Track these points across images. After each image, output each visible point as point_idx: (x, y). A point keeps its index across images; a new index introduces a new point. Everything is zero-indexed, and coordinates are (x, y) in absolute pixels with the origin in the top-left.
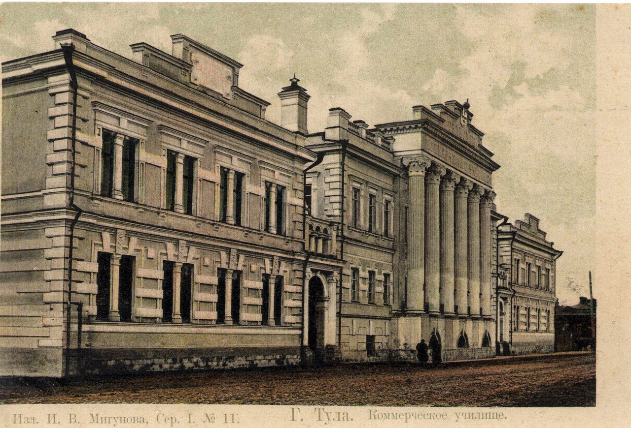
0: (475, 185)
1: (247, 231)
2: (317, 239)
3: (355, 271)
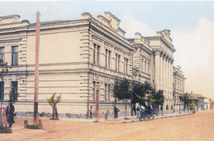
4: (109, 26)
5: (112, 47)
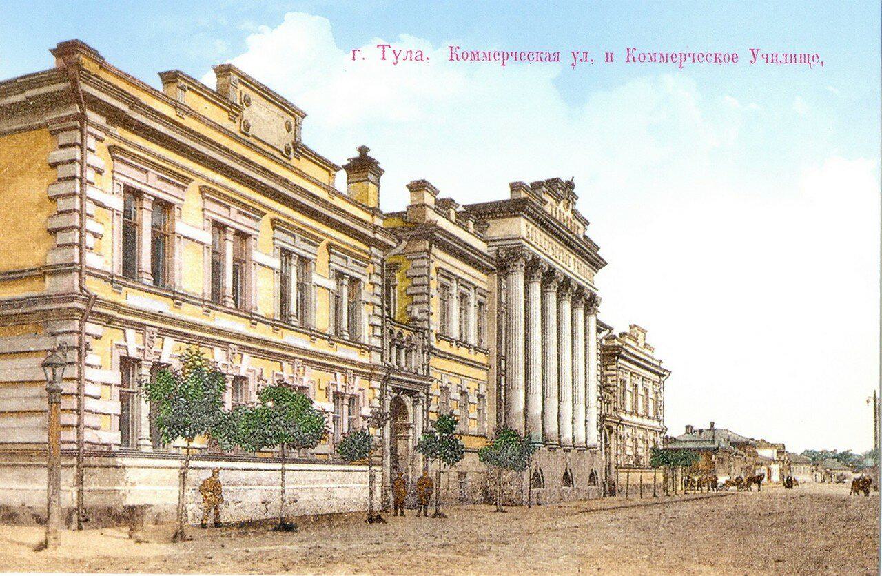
0: (566, 277)
1: (207, 306)
2: (399, 348)
3: (444, 389)
4: (234, 128)
5: (258, 220)
